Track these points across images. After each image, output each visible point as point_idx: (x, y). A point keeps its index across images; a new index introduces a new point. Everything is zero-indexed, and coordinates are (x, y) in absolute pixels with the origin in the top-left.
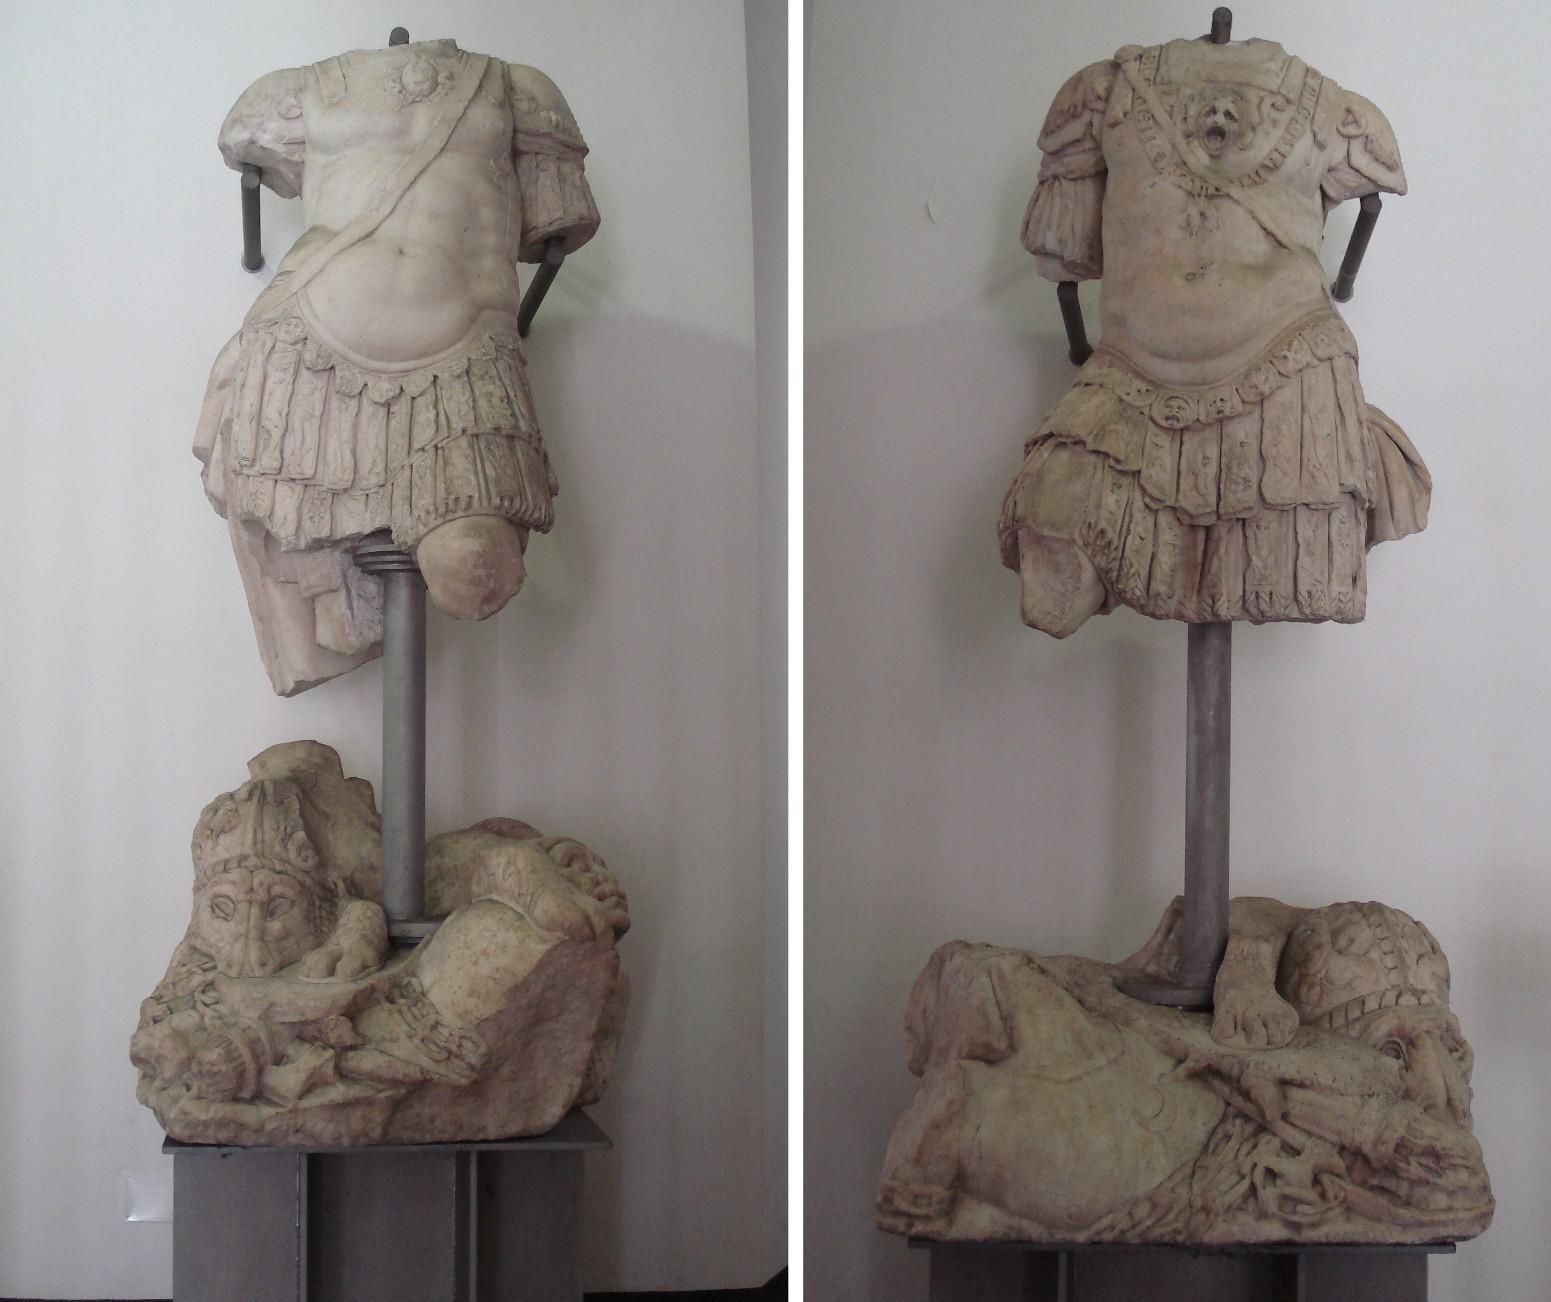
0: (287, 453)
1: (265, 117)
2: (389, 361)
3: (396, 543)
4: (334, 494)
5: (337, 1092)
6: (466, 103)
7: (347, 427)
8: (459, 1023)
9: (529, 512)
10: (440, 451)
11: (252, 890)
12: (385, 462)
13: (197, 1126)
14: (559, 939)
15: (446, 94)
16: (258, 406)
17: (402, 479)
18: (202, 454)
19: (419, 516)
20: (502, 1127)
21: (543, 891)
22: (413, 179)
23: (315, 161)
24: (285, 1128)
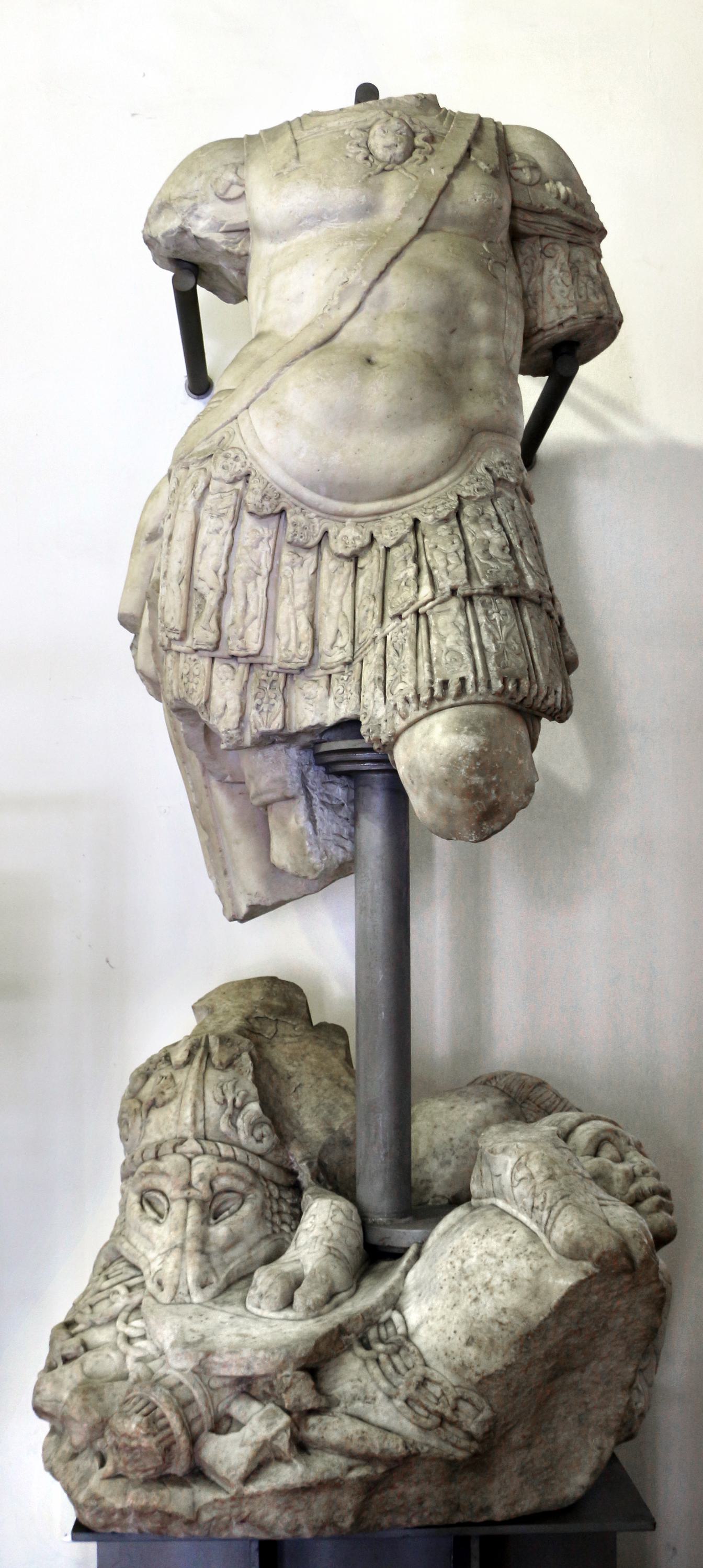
0: (226, 622)
1: (198, 200)
2: (356, 501)
3: (366, 739)
4: (287, 675)
5: (288, 1474)
6: (450, 170)
7: (302, 587)
8: (454, 1380)
9: (541, 698)
10: (422, 620)
11: (189, 1185)
12: (351, 631)
13: (113, 1514)
14: (586, 1272)
15: (426, 159)
16: (189, 563)
17: (373, 656)
18: (129, 622)
19: (395, 705)
20: (513, 1504)
21: (566, 1205)
22: (383, 268)
23: (262, 252)
24: (226, 1518)
